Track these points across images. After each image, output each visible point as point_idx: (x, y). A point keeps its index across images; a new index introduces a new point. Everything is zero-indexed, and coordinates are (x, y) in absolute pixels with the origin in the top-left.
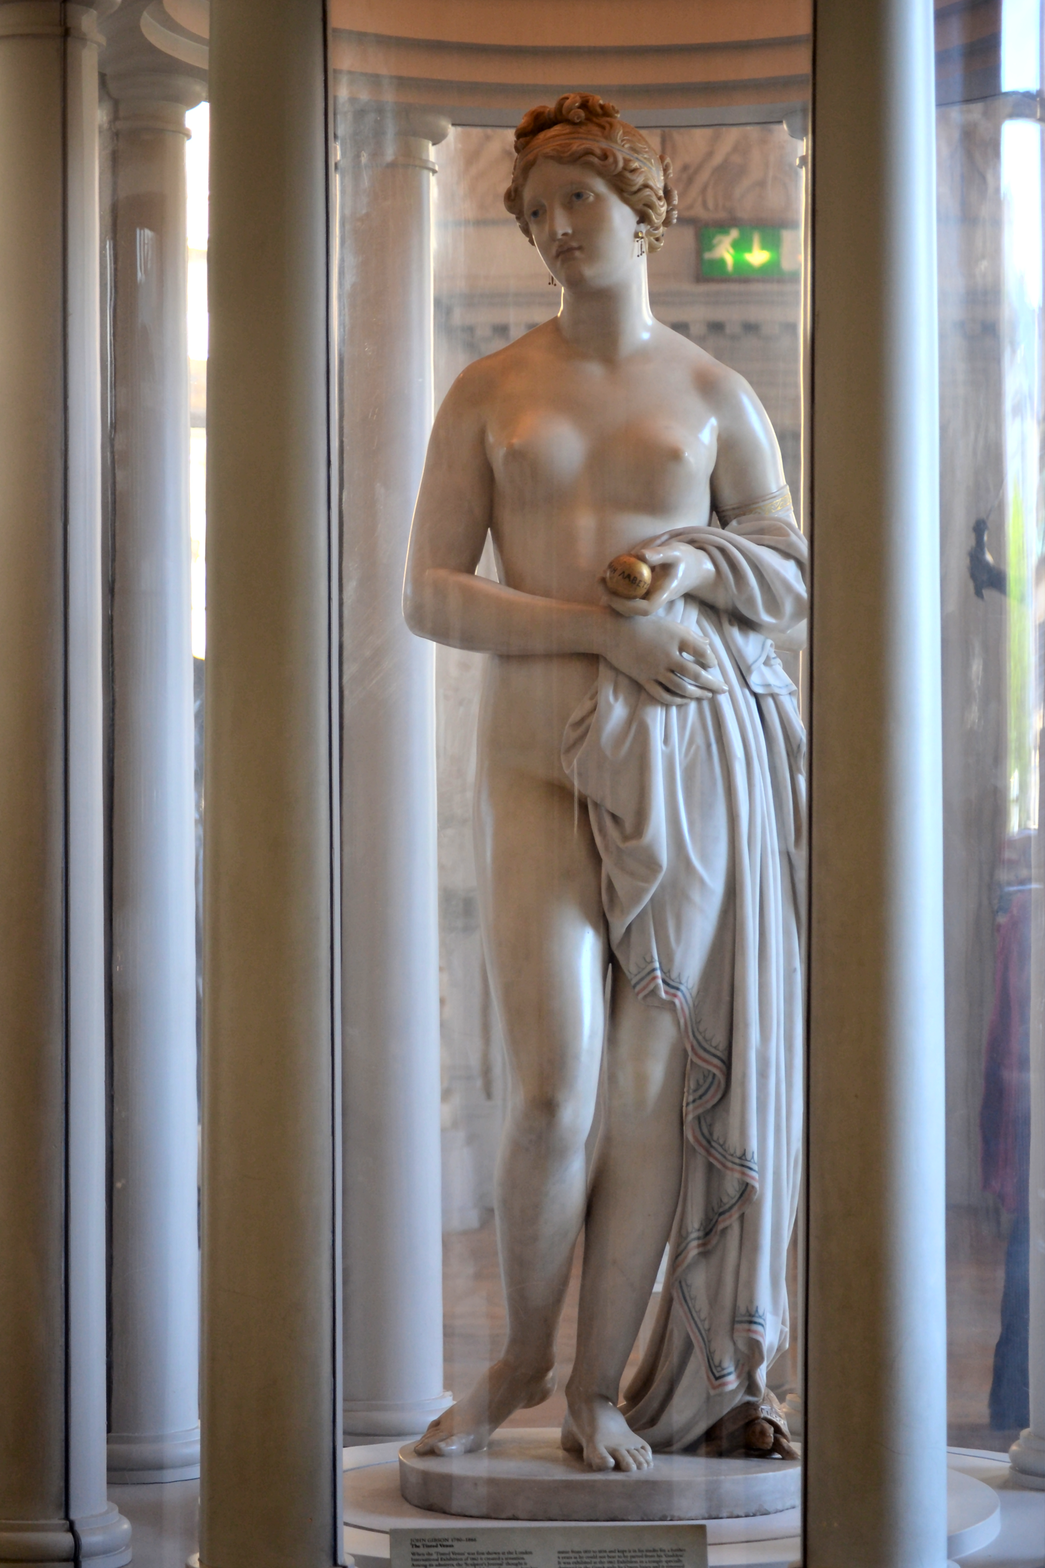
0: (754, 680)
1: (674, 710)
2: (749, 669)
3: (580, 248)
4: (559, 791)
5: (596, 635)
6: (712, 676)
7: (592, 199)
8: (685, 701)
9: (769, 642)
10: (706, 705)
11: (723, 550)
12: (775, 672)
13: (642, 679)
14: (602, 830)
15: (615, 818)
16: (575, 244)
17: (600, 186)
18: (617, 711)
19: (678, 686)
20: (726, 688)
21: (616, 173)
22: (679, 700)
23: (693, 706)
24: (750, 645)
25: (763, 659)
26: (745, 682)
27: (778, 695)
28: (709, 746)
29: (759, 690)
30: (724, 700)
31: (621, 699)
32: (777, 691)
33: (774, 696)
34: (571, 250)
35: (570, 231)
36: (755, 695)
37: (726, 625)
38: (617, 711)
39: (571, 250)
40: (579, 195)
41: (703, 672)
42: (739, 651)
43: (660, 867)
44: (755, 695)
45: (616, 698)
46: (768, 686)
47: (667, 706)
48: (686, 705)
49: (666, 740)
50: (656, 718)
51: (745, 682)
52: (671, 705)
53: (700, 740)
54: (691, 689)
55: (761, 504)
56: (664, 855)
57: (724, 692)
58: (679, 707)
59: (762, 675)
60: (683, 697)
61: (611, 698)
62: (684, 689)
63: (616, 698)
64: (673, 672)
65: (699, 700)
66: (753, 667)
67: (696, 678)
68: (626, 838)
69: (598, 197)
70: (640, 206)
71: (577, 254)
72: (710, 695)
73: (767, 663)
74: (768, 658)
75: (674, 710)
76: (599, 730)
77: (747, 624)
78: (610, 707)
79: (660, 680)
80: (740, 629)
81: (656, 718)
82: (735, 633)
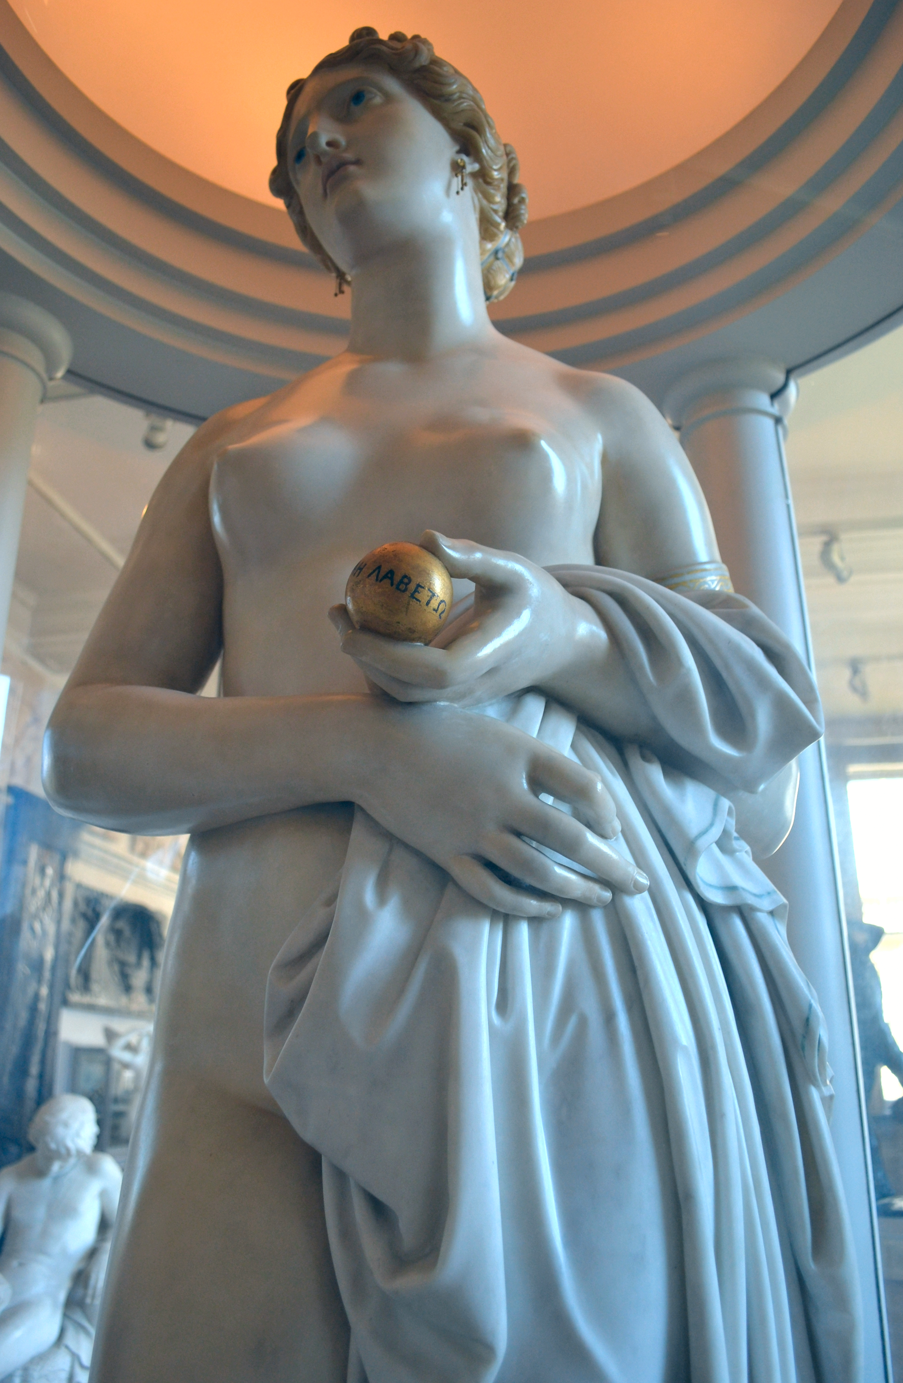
0: (704, 872)
1: (523, 930)
2: (691, 848)
3: (358, 162)
4: (267, 1126)
5: (338, 761)
6: (613, 852)
7: (378, 100)
8: (547, 907)
9: (725, 803)
10: (598, 919)
11: (622, 600)
12: (741, 865)
13: (442, 854)
14: (348, 1233)
15: (379, 1209)
16: (349, 156)
17: (392, 85)
18: (383, 928)
19: (529, 865)
20: (644, 880)
21: (417, 65)
22: (533, 905)
23: (568, 922)
24: (691, 805)
25: (716, 832)
26: (686, 882)
27: (753, 909)
28: (609, 1018)
29: (716, 897)
30: (640, 908)
31: (393, 905)
32: (751, 900)
33: (744, 912)
34: (343, 164)
35: (343, 141)
36: (704, 905)
37: (636, 762)
38: (383, 928)
39: (343, 164)
40: (358, 98)
41: (591, 838)
42: (667, 811)
43: (490, 1349)
44: (704, 905)
45: (382, 899)
46: (731, 889)
47: (506, 919)
48: (551, 918)
49: (505, 1001)
50: (479, 951)
51: (686, 882)
52: (518, 918)
53: (589, 1004)
54: (562, 873)
55: (687, 577)
56: (499, 1316)
57: (639, 889)
58: (535, 921)
59: (719, 867)
60: (543, 895)
61: (369, 897)
62: (543, 874)
63: (382, 899)
64: (518, 834)
65: (581, 906)
66: (702, 843)
67: (569, 848)
68: (401, 1261)
69: (389, 98)
70: (459, 125)
71: (352, 168)
72: (608, 895)
73: (723, 844)
74: (725, 833)
75: (523, 930)
76: (335, 976)
77: (680, 764)
78: (364, 919)
79: (489, 862)
80: (666, 774)
81: (479, 951)
82: (655, 773)
